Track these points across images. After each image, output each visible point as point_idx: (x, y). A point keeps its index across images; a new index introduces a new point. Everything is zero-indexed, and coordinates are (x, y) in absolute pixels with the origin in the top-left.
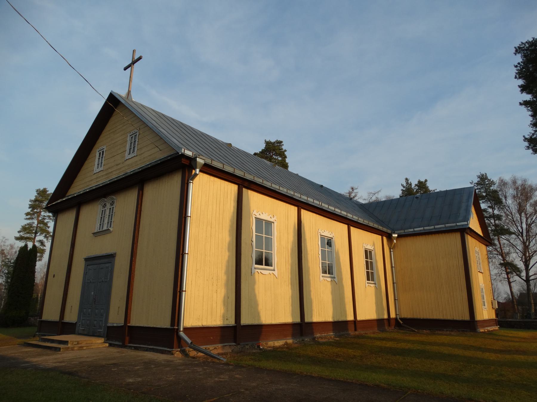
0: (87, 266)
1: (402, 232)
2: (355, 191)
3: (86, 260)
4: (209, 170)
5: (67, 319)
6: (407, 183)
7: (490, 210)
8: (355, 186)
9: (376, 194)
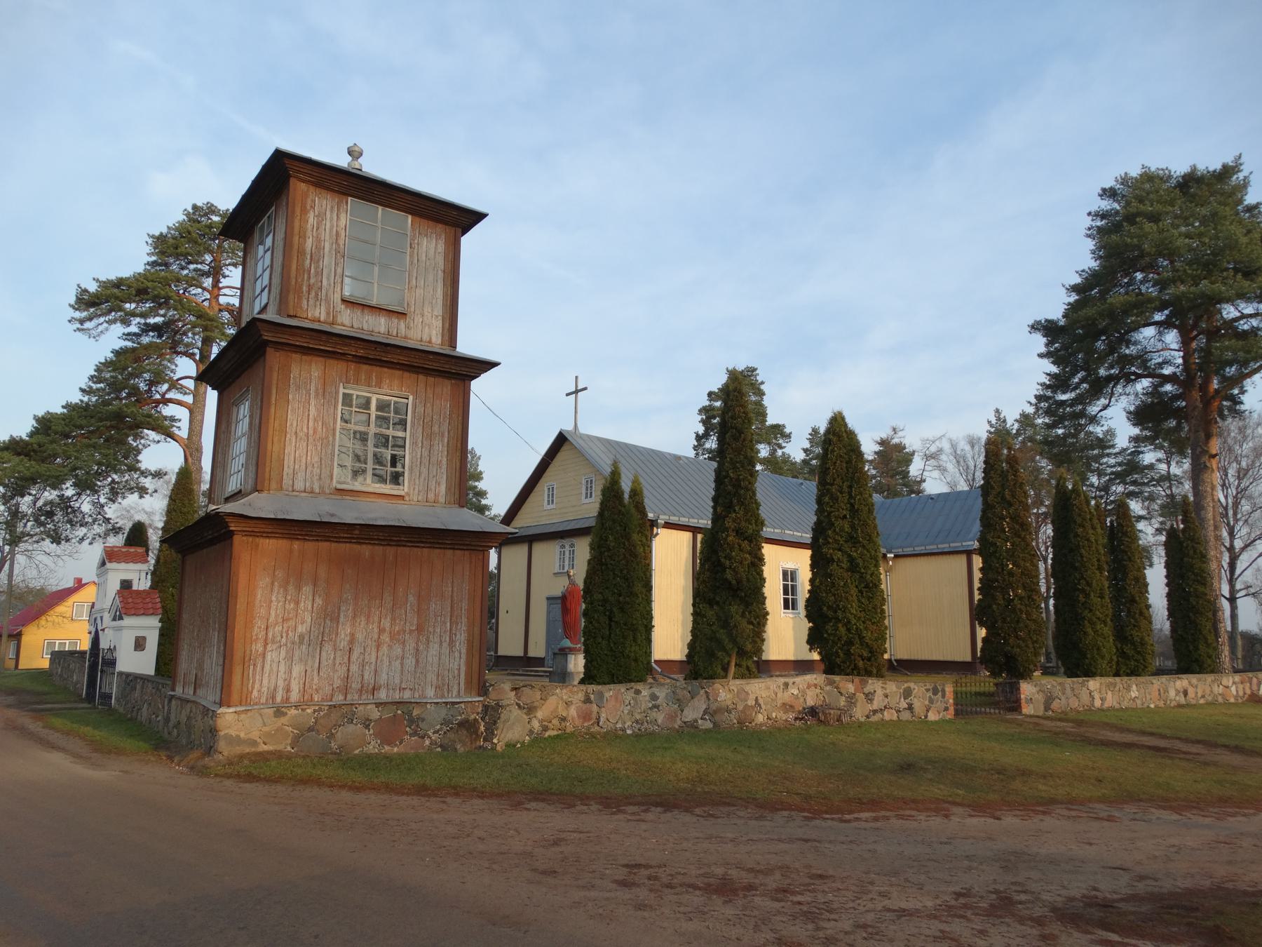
0: (549, 605)
1: (900, 551)
2: (900, 434)
3: (548, 599)
4: (668, 525)
5: (531, 654)
6: (998, 419)
7: (1163, 466)
8: (900, 425)
9: (937, 443)
